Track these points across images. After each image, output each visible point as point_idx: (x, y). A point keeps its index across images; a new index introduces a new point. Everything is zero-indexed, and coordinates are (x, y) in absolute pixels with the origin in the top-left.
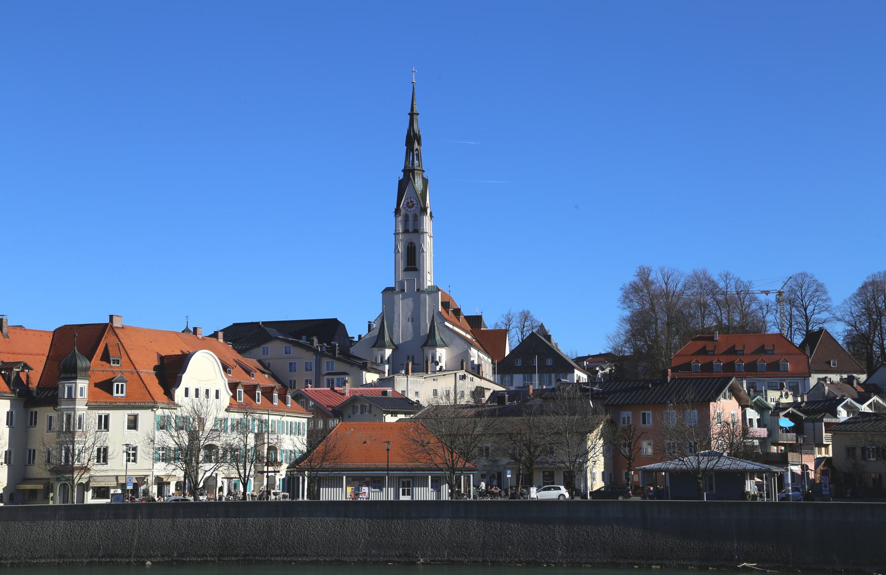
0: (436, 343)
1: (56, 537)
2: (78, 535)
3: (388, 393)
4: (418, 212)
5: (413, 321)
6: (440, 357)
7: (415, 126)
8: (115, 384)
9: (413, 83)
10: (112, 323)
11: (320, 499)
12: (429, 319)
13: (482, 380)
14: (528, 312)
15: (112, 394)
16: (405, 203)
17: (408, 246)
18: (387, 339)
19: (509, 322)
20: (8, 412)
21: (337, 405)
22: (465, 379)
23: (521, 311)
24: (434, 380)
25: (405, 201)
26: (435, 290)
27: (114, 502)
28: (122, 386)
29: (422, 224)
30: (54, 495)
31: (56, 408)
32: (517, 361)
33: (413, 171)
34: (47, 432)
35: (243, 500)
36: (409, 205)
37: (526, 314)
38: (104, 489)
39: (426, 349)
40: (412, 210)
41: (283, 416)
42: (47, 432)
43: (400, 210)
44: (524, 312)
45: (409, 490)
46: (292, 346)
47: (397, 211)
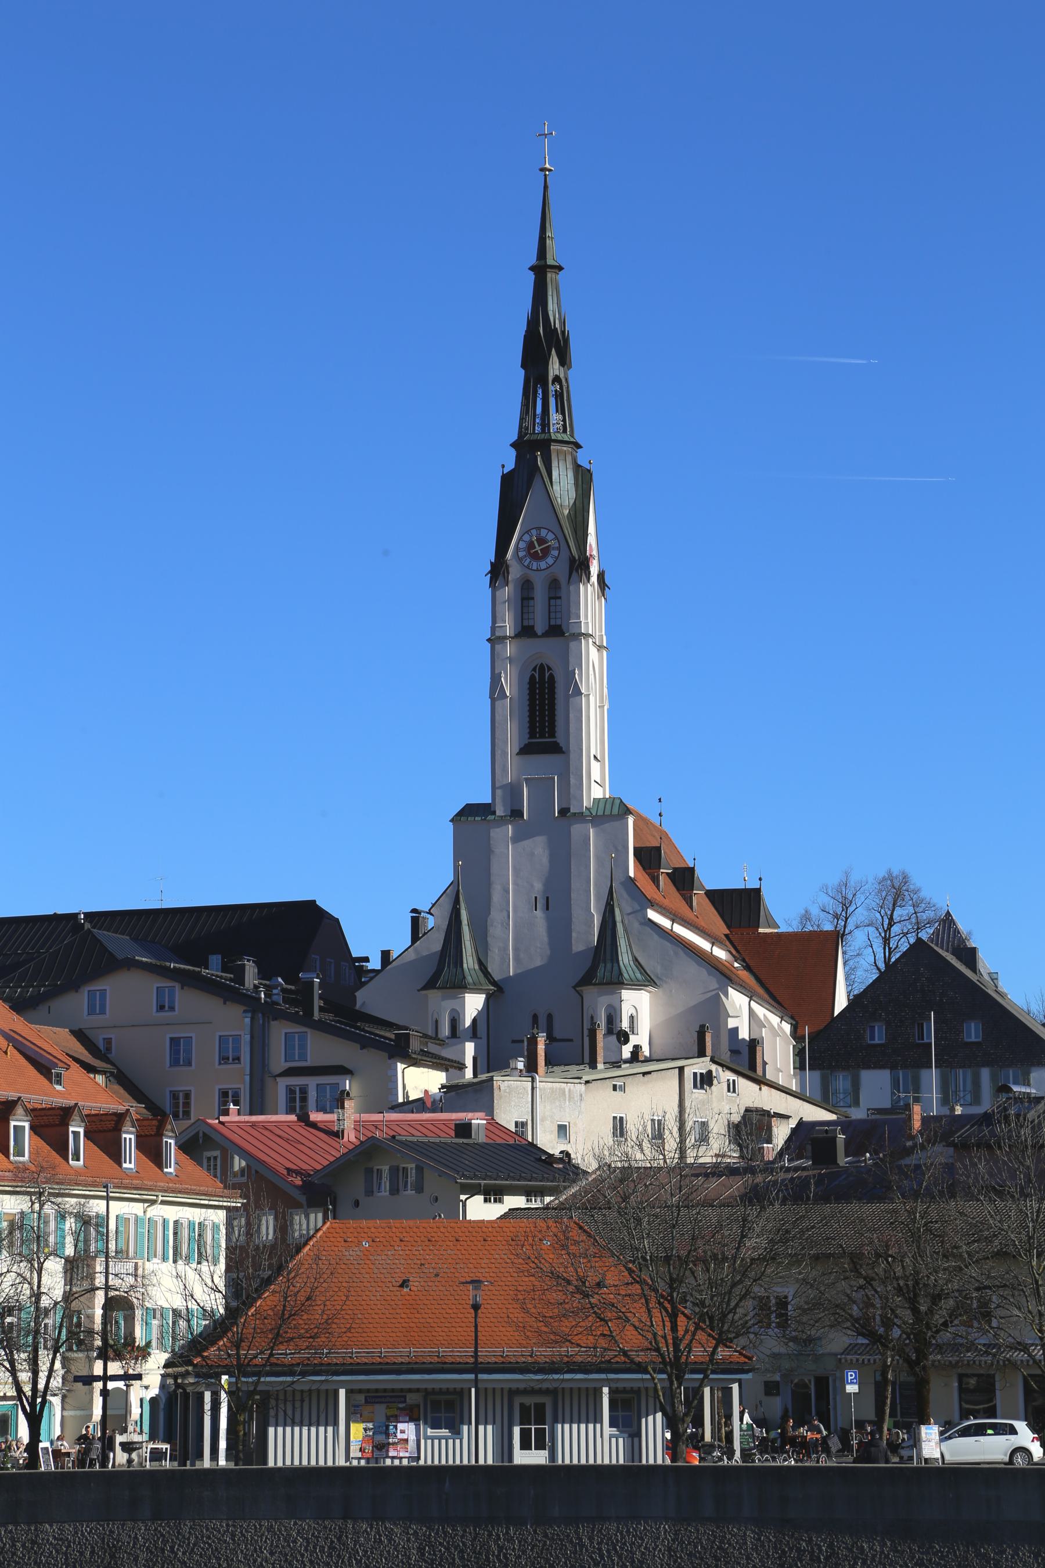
0: (621, 974)
4: (561, 571)
5: (547, 909)
6: (632, 1017)
9: (543, 170)
13: (765, 1088)
14: (905, 879)
16: (522, 545)
18: (469, 961)
19: (845, 907)
22: (710, 1084)
23: (882, 873)
24: (615, 1088)
25: (520, 539)
26: (615, 811)
29: (573, 610)
36: (536, 552)
37: (897, 885)
40: (543, 565)
41: (153, 1202)
43: (507, 567)
44: (890, 877)
45: (540, 1433)
46: (177, 986)
47: (498, 571)
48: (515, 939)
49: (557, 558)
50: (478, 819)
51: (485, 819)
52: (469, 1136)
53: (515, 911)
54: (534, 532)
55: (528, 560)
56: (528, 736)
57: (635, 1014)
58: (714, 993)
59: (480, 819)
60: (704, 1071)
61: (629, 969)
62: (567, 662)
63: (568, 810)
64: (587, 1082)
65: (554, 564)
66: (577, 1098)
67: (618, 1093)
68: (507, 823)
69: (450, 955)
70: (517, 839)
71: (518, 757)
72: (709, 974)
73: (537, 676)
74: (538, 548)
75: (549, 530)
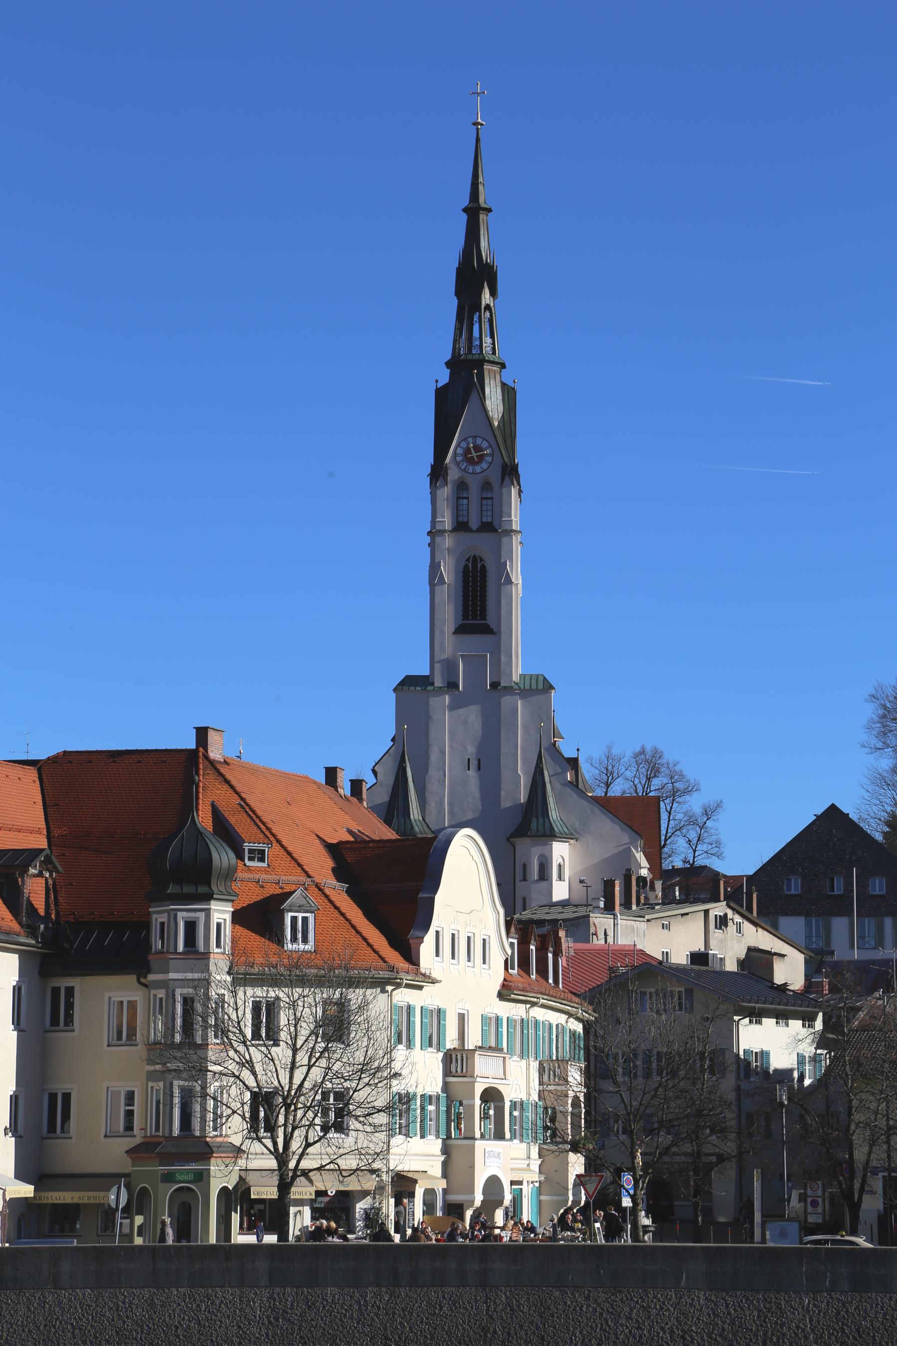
0: (552, 828)
1: (691, 1336)
2: (756, 1335)
3: (710, 958)
4: (494, 476)
5: (479, 769)
6: (560, 866)
7: (484, 244)
8: (288, 917)
9: (476, 124)
10: (206, 749)
11: (231, 1242)
12: (524, 761)
13: (760, 930)
15: (280, 942)
16: (460, 451)
17: (466, 567)
20: (14, 987)
21: (595, 985)
22: (726, 926)
25: (458, 446)
26: (541, 686)
27: (772, 1240)
28: (305, 920)
29: (505, 509)
30: (145, 1219)
31: (142, 980)
32: (789, 881)
33: (480, 363)
34: (108, 1045)
35: (762, 1243)
36: (471, 458)
38: (262, 1207)
39: (522, 844)
40: (478, 469)
42: (108, 1045)
43: (446, 469)
44: (643, 752)
47: (437, 473)
48: (450, 795)
49: (491, 463)
50: (418, 688)
51: (425, 689)
52: (707, 964)
53: (450, 771)
54: (470, 440)
55: (465, 464)
56: (462, 618)
57: (562, 863)
58: (628, 845)
59: (420, 689)
60: (722, 914)
61: (558, 824)
62: (498, 554)
63: (498, 684)
64: (648, 920)
65: (488, 468)
66: (642, 935)
67: (666, 931)
68: (444, 693)
69: (398, 807)
70: (453, 707)
71: (454, 636)
72: (622, 830)
73: (470, 566)
74: (474, 454)
75: (484, 439)
